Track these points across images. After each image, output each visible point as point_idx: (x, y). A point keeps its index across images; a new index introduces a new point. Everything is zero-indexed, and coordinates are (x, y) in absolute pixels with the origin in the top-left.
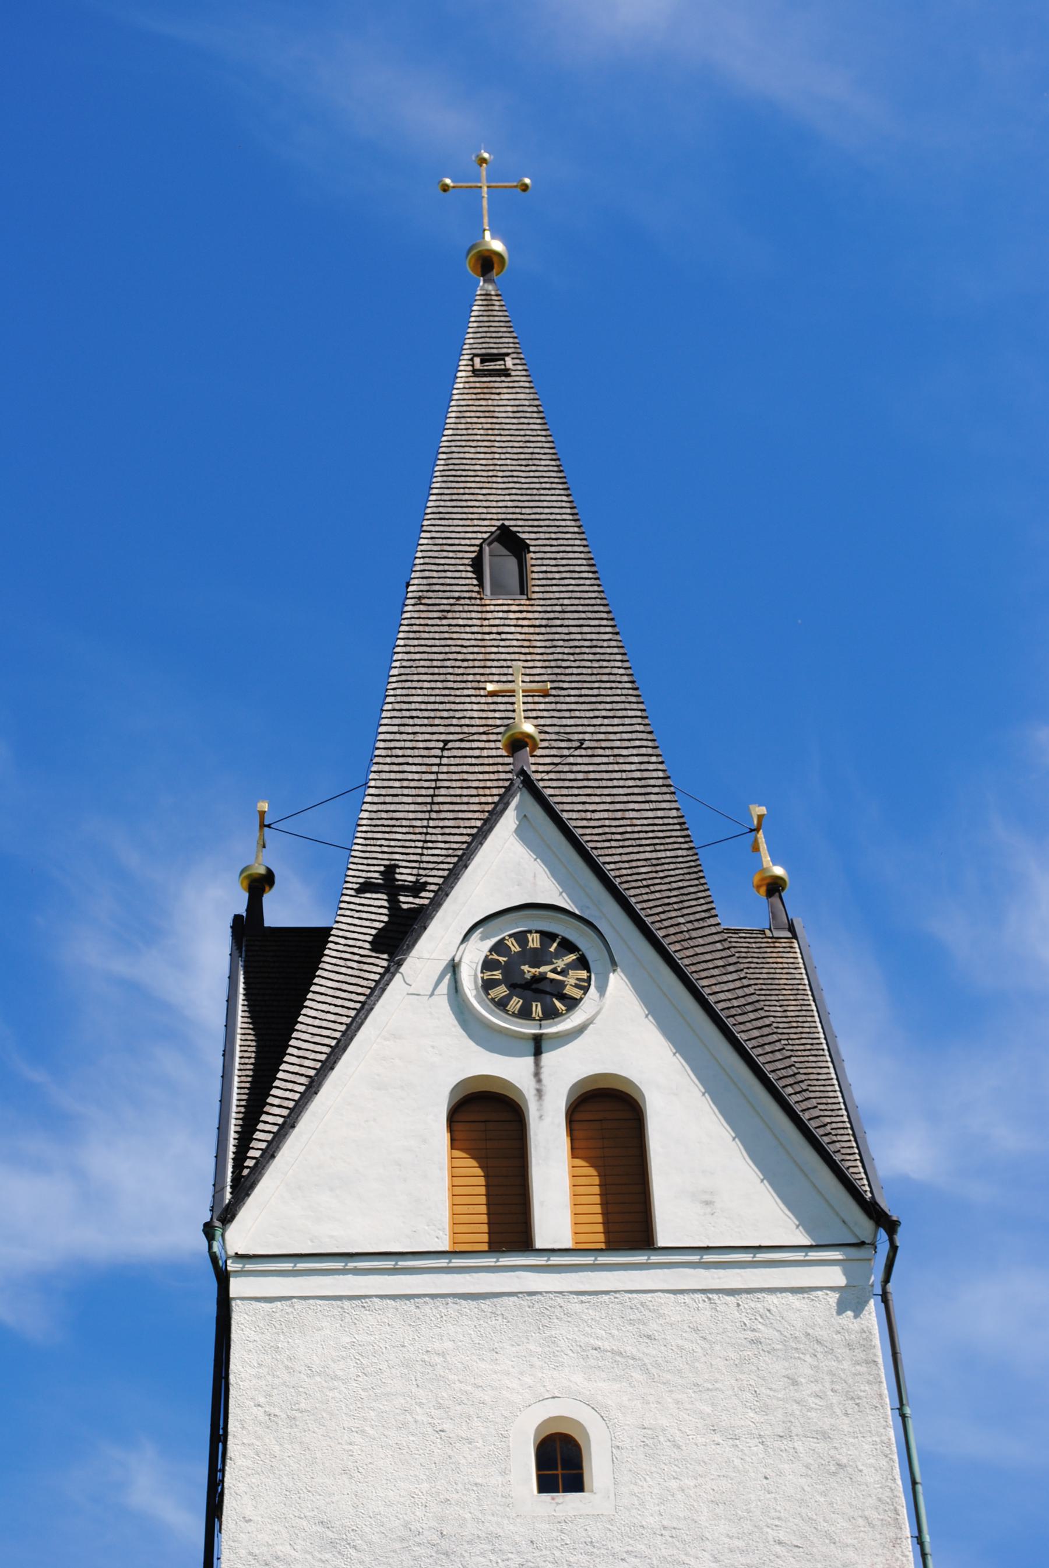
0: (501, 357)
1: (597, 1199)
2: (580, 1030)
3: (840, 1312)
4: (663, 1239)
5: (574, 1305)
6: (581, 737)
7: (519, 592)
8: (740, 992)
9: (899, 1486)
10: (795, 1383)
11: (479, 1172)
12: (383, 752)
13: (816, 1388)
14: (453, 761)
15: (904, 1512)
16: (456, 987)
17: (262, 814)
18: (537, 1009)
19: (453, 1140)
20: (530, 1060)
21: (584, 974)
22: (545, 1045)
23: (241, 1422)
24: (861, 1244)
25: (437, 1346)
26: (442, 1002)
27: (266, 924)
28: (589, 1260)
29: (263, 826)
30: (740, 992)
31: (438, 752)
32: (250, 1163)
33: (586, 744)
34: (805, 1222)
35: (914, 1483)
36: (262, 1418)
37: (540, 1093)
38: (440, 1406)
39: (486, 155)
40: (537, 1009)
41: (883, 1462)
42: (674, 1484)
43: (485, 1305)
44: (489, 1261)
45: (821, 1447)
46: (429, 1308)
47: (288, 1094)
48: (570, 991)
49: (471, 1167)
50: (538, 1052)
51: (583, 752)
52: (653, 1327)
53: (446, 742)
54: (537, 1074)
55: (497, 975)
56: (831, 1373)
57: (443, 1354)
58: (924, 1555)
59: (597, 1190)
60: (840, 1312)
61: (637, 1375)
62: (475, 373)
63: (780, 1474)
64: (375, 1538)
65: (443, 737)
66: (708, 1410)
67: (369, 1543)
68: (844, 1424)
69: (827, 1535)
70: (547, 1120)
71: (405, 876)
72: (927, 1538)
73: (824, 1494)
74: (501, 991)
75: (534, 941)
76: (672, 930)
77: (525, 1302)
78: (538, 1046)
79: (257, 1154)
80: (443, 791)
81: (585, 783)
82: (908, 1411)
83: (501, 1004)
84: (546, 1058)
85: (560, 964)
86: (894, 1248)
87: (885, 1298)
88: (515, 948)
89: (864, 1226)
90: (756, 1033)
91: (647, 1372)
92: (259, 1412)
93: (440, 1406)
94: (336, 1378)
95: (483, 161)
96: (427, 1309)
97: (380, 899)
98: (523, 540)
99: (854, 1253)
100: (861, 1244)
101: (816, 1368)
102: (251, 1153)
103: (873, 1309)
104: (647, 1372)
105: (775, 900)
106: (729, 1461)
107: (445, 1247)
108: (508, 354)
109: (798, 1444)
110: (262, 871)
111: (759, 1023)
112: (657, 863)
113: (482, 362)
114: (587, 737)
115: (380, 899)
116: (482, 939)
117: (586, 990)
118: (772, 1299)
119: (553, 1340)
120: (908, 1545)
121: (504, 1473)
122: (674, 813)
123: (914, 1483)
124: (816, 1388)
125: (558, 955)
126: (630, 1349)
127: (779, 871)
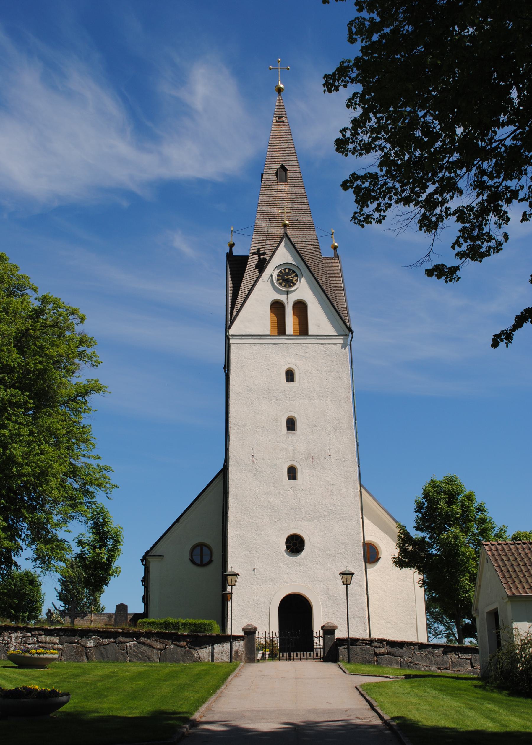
0: (282, 117)
1: (298, 324)
2: (296, 290)
3: (342, 348)
5: (293, 346)
8: (327, 279)
9: (350, 381)
10: (333, 362)
11: (276, 318)
12: (257, 221)
13: (336, 363)
14: (271, 223)
15: (351, 386)
17: (232, 230)
18: (287, 285)
19: (271, 311)
20: (286, 296)
21: (297, 278)
22: (289, 293)
24: (346, 335)
25: (268, 353)
26: (269, 283)
27: (233, 254)
28: (296, 337)
29: (232, 232)
30: (327, 279)
31: (268, 221)
32: (233, 318)
34: (337, 331)
35: (353, 381)
37: (288, 303)
38: (268, 365)
39: (280, 60)
40: (287, 285)
41: (348, 377)
42: (310, 380)
43: (277, 345)
44: (278, 337)
46: (266, 346)
47: (240, 301)
48: (294, 281)
49: (275, 317)
50: (287, 294)
51: (298, 222)
52: (307, 350)
53: (270, 219)
54: (287, 299)
55: (280, 278)
56: (339, 360)
57: (269, 355)
58: (354, 394)
59: (298, 322)
60: (342, 348)
61: (304, 360)
62: (277, 121)
63: (329, 379)
66: (317, 367)
67: (256, 390)
68: (341, 370)
71: (262, 251)
72: (354, 391)
73: (337, 383)
74: (281, 281)
75: (287, 271)
76: (314, 265)
77: (284, 345)
78: (288, 293)
79: (234, 316)
80: (269, 231)
82: (353, 367)
83: (281, 284)
84: (289, 295)
85: (292, 276)
86: (352, 337)
87: (350, 345)
88: (284, 272)
89: (347, 331)
90: (329, 289)
93: (268, 365)
94: (250, 359)
95: (279, 61)
96: (266, 346)
97: (256, 257)
98: (285, 167)
99: (345, 337)
100: (346, 335)
101: (336, 359)
102: (233, 316)
103: (348, 348)
105: (335, 251)
107: (269, 334)
108: (284, 116)
109: (333, 373)
110: (232, 243)
111: (330, 287)
112: (311, 249)
113: (278, 118)
115: (256, 257)
116: (277, 270)
117: (297, 281)
118: (329, 345)
120: (351, 393)
121: (280, 378)
122: (316, 237)
123: (353, 381)
124: (336, 363)
125: (292, 274)
127: (336, 244)
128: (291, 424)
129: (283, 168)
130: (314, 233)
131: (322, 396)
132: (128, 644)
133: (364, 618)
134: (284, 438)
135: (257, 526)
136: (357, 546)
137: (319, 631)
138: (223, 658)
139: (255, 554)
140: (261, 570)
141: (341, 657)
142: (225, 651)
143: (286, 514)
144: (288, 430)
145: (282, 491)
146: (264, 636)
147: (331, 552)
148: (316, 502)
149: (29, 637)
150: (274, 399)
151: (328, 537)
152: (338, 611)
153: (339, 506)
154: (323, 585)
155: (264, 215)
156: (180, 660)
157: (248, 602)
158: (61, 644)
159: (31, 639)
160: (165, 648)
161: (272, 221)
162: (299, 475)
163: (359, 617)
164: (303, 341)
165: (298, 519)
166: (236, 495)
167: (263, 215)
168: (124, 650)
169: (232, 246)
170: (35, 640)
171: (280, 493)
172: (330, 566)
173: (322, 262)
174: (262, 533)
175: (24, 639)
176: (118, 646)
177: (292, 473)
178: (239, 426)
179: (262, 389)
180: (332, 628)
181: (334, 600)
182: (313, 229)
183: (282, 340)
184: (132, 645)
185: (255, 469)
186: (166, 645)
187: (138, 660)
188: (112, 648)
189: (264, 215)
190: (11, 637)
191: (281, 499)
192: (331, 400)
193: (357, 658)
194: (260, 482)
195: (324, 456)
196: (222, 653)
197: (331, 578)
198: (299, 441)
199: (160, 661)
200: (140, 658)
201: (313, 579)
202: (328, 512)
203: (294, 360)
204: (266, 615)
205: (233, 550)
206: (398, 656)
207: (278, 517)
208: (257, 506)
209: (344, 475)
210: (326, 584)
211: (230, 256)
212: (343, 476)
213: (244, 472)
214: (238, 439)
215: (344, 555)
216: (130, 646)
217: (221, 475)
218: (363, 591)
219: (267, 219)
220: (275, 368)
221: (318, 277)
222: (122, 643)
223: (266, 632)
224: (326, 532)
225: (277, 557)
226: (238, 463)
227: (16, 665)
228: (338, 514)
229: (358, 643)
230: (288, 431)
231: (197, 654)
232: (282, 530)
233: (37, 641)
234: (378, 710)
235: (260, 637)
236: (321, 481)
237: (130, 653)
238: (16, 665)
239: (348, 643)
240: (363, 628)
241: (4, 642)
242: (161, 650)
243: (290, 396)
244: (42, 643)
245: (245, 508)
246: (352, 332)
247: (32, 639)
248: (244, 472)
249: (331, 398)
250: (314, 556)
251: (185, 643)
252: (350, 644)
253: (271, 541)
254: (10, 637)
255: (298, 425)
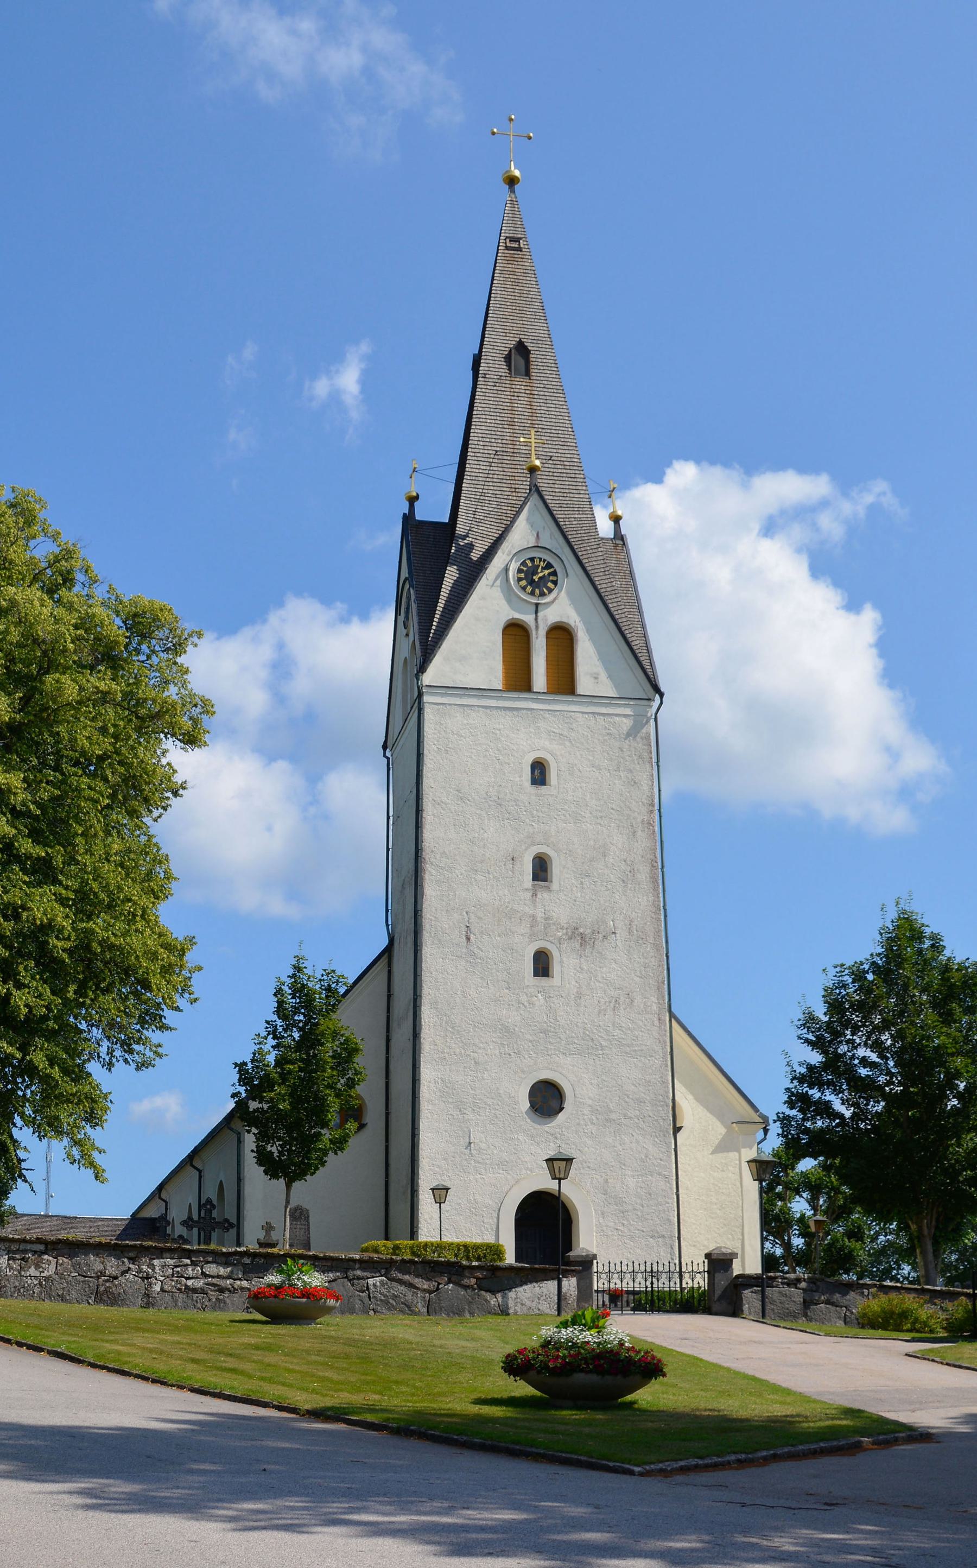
2: (553, 602)
4: (580, 690)
6: (551, 454)
7: (524, 373)
10: (622, 751)
16: (507, 580)
18: (537, 592)
22: (540, 608)
23: (429, 750)
27: (447, 521)
31: (492, 456)
33: (553, 458)
34: (617, 686)
36: (436, 749)
38: (498, 750)
40: (537, 592)
42: (578, 785)
45: (629, 775)
51: (551, 462)
53: (496, 451)
54: (536, 619)
55: (522, 575)
56: (635, 748)
57: (500, 730)
61: (567, 743)
62: (507, 248)
63: (615, 784)
64: (476, 797)
65: (495, 449)
66: (591, 758)
67: (474, 799)
69: (629, 807)
70: (539, 639)
73: (629, 792)
74: (524, 583)
81: (552, 478)
83: (524, 588)
86: (661, 703)
91: (571, 742)
92: (435, 747)
93: (498, 750)
100: (649, 699)
104: (571, 742)
106: (597, 778)
109: (621, 773)
110: (415, 494)
113: (510, 241)
114: (554, 454)
119: (538, 728)
126: (565, 733)
128: (541, 869)
129: (522, 349)
130: (584, 488)
131: (601, 817)
132: (371, 1281)
133: (671, 1237)
134: (528, 895)
135: (476, 1062)
136: (662, 1106)
137: (704, 1262)
138: (540, 1308)
139: (472, 1117)
140: (483, 1146)
141: (746, 1307)
142: (544, 1294)
143: (531, 1041)
144: (533, 880)
145: (523, 998)
146: (643, 1269)
147: (613, 1116)
148: (587, 1022)
149: (187, 1265)
150: (508, 819)
151: (608, 1087)
152: (623, 1224)
153: (629, 1029)
154: (597, 1177)
155: (485, 444)
156: (464, 1311)
157: (459, 1204)
158: (247, 1281)
159: (190, 1269)
160: (438, 1289)
161: (500, 457)
162: (556, 968)
163: (663, 1236)
164: (563, 705)
165: (553, 1052)
166: (436, 1003)
167: (481, 443)
168: (363, 1292)
169: (412, 500)
170: (198, 1271)
171: (519, 1002)
172: (611, 1141)
173: (600, 549)
174: (486, 1076)
175: (179, 1269)
176: (353, 1285)
177: (542, 966)
178: (442, 868)
179: (485, 796)
180: (728, 1257)
181: (616, 1205)
182: (582, 480)
183: (521, 702)
184: (378, 1284)
185: (473, 954)
186: (439, 1284)
187: (389, 1309)
188: (341, 1288)
189: (485, 444)
190: (153, 1265)
191: (522, 1012)
192: (618, 826)
193: (773, 1310)
194: (482, 978)
195: (604, 934)
196: (539, 1299)
197: (613, 1164)
198: (556, 903)
199: (428, 1312)
200: (393, 1306)
201: (580, 1165)
202: (609, 1040)
203: (547, 743)
204: (492, 1229)
205: (430, 1107)
206: (841, 1307)
207: (515, 1046)
208: (477, 1024)
209: (640, 972)
210: (603, 1175)
211: (409, 520)
212: (638, 974)
213: (451, 957)
214: (438, 893)
215: (637, 1121)
216: (374, 1285)
217: (384, 960)
218: (671, 1189)
219: (491, 452)
220: (511, 757)
221: (596, 579)
222: (359, 1278)
223: (646, 1263)
224: (604, 1078)
225: (512, 1123)
226: (439, 940)
227: (264, 1318)
228: (628, 1046)
229: (775, 1283)
230: (536, 882)
231: (495, 1299)
232: (523, 1072)
233: (203, 1273)
234: (498, 1408)
235: (624, 1271)
236: (598, 981)
237: (374, 1297)
238: (264, 1318)
239: (763, 1282)
240: (669, 1255)
241: (141, 1275)
242: (430, 1292)
243: (541, 815)
244: (213, 1277)
245: (453, 1028)
246: (662, 695)
247: (193, 1270)
248: (451, 957)
249: (617, 822)
250: (582, 1122)
251: (473, 1281)
252: (765, 1285)
253: (501, 1092)
254: (153, 1267)
255: (556, 870)
